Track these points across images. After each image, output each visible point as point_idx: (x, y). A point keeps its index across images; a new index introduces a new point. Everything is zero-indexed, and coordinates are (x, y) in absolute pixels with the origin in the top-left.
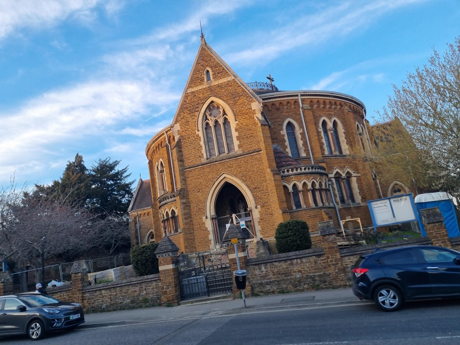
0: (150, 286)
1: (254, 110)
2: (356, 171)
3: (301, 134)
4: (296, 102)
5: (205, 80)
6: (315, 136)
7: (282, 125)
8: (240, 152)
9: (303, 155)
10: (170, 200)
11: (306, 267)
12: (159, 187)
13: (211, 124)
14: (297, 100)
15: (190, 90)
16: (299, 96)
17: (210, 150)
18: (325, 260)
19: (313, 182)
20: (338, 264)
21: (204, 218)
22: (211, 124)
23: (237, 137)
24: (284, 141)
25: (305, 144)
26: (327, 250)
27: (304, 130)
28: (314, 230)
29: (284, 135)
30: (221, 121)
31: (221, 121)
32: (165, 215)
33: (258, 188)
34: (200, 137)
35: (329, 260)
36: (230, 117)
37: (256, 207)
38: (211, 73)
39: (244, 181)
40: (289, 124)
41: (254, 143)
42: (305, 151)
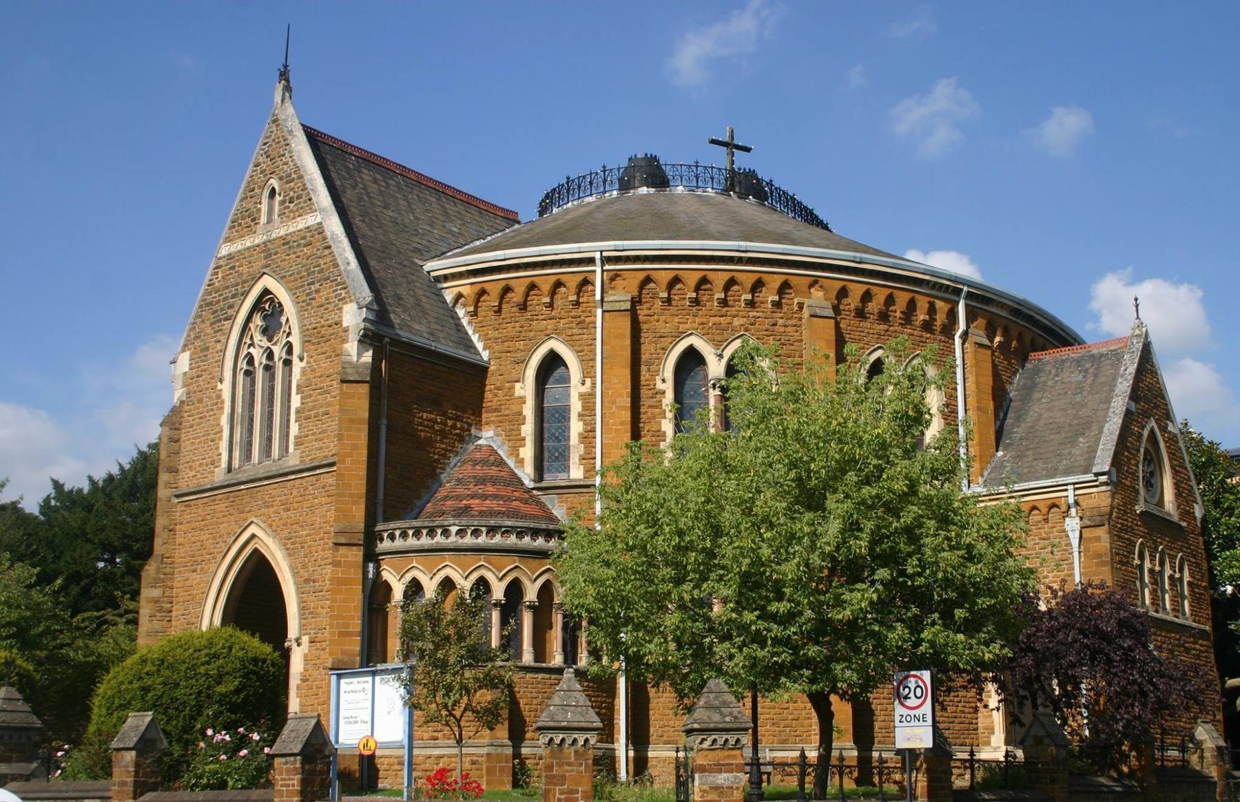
3: (581, 396)
5: (263, 219)
6: (623, 408)
7: (524, 362)
14: (590, 277)
24: (519, 419)
28: (440, 735)
29: (522, 400)
34: (223, 402)
39: (290, 555)
40: (552, 362)
42: (582, 458)
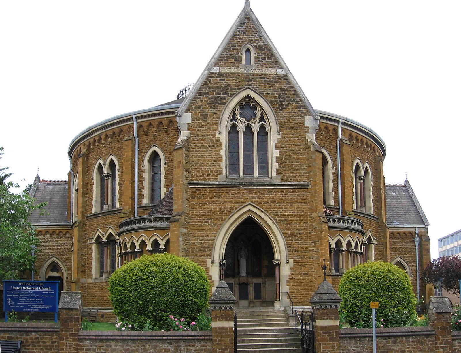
0: (193, 346)
1: (307, 127)
2: (376, 237)
4: (335, 131)
5: (243, 62)
8: (277, 180)
9: (332, 203)
10: (153, 224)
11: (411, 347)
12: (96, 198)
13: (241, 128)
14: (336, 128)
15: (217, 70)
16: (340, 123)
17: (234, 167)
18: (432, 341)
19: (349, 241)
20: (447, 347)
21: (209, 261)
22: (241, 128)
23: (277, 158)
25: (336, 189)
26: (439, 330)
27: (337, 170)
30: (256, 128)
31: (256, 128)
32: (129, 246)
33: (295, 236)
34: (221, 144)
35: (439, 342)
36: (273, 127)
37: (288, 262)
38: (253, 55)
41: (299, 173)
